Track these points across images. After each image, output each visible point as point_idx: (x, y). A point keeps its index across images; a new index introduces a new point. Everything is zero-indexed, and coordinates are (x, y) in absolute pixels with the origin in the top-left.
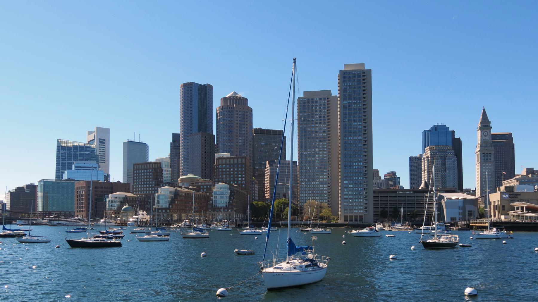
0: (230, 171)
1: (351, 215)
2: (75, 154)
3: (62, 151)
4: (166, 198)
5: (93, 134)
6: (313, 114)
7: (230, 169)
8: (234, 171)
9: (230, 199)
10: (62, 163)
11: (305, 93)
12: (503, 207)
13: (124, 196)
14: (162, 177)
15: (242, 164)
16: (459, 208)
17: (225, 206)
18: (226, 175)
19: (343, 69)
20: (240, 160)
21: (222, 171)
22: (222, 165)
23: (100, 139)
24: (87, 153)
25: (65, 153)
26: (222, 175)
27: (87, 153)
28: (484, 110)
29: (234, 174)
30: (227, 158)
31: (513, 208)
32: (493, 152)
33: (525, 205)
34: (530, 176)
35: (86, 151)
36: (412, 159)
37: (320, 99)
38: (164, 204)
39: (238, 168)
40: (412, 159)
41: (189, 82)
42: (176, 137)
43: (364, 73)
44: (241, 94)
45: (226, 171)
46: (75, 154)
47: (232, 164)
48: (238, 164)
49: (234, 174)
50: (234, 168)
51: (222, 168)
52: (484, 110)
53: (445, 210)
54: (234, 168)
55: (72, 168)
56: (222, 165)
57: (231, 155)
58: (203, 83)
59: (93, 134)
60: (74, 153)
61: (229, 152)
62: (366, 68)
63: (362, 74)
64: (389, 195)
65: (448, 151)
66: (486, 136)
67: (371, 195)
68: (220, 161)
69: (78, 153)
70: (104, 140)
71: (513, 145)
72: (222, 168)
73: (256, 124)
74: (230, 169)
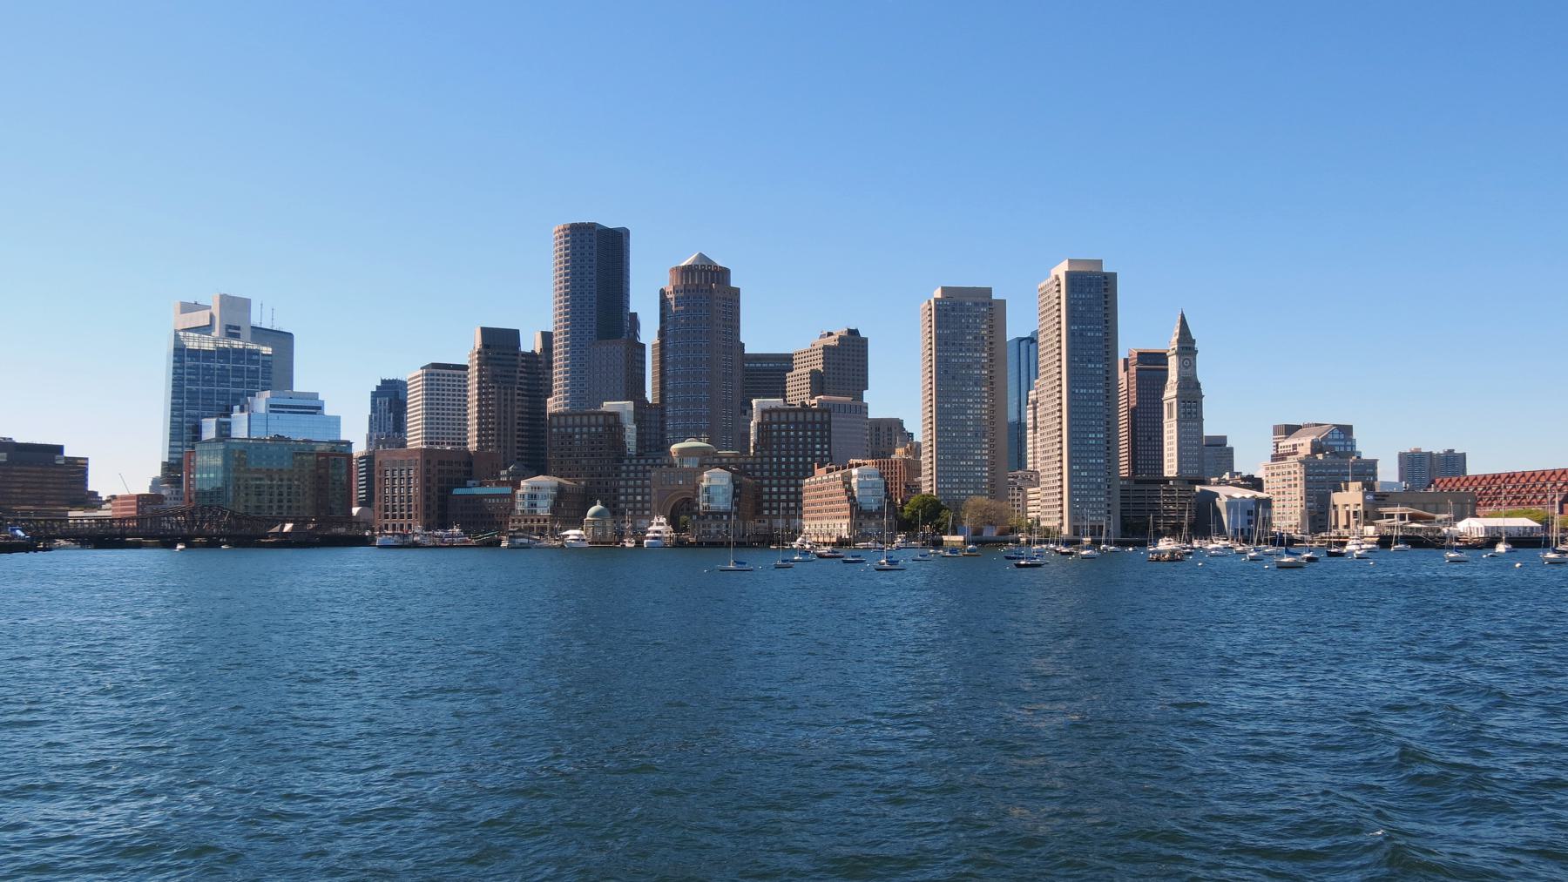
0: (797, 436)
2: (223, 368)
3: (188, 362)
4: (725, 491)
5: (207, 312)
8: (805, 437)
9: (798, 493)
10: (189, 391)
12: (1366, 513)
17: (875, 507)
18: (788, 444)
21: (779, 436)
23: (229, 327)
24: (253, 367)
25: (197, 367)
26: (779, 445)
27: (253, 367)
29: (805, 443)
31: (1380, 516)
33: (1408, 511)
34: (1320, 456)
35: (251, 361)
37: (976, 304)
38: (722, 502)
39: (813, 432)
44: (720, 262)
45: (788, 436)
46: (223, 368)
49: (805, 443)
51: (779, 431)
53: (1225, 516)
54: (805, 431)
56: (779, 423)
59: (207, 312)
60: (217, 365)
62: (1105, 269)
69: (229, 366)
70: (238, 328)
71: (1198, 385)
72: (779, 431)
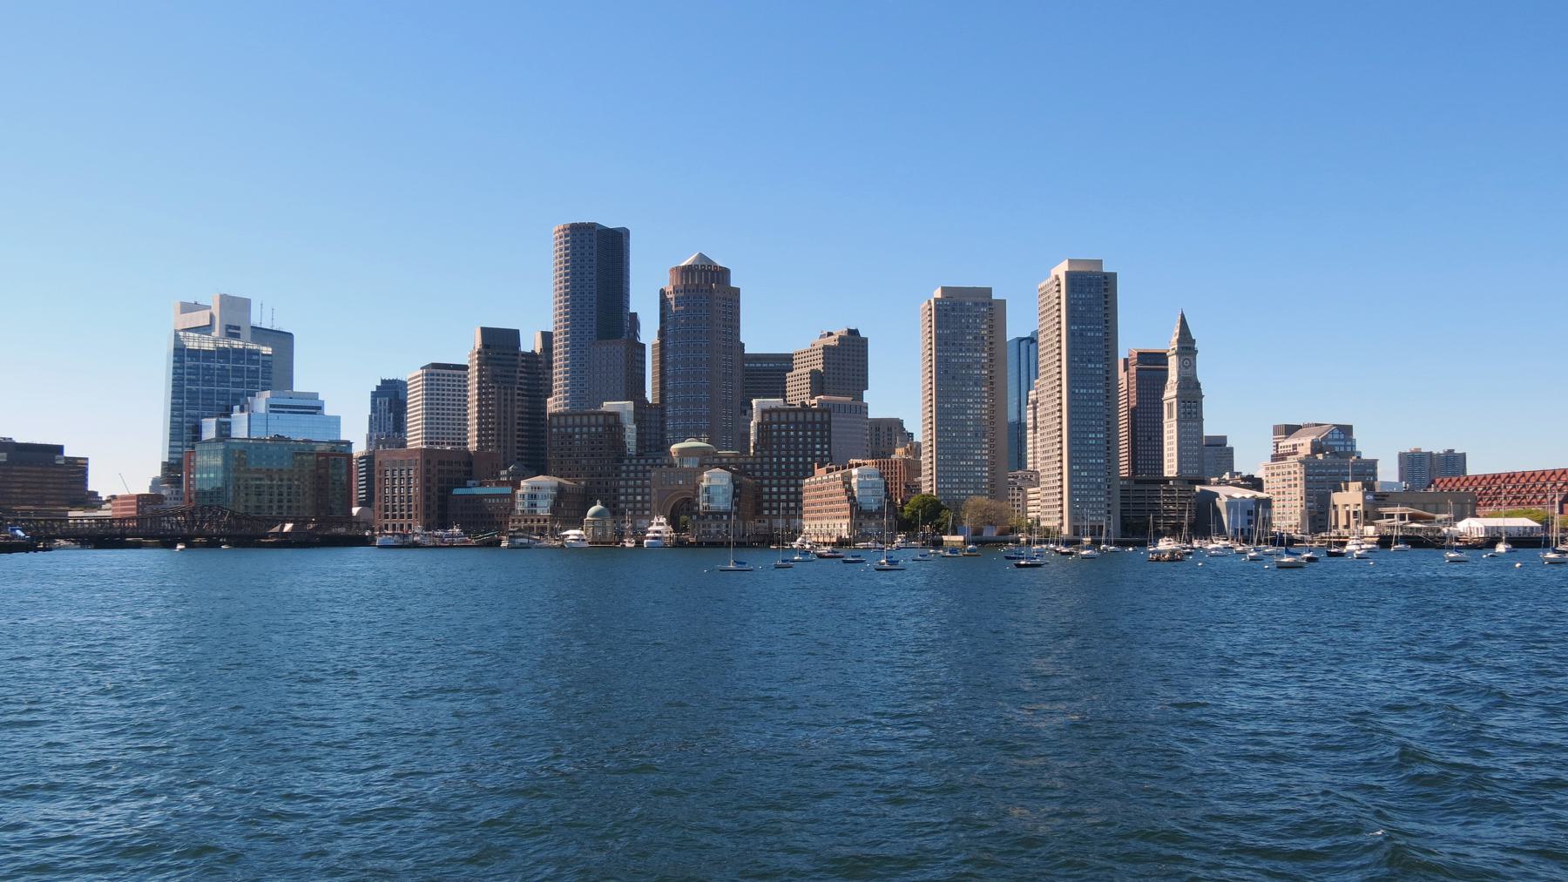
0: (797, 436)
2: (223, 368)
3: (188, 362)
4: (725, 491)
5: (207, 312)
8: (805, 437)
9: (798, 493)
10: (189, 391)
12: (1366, 513)
17: (875, 507)
18: (788, 444)
21: (779, 436)
23: (229, 327)
24: (253, 367)
25: (197, 367)
26: (779, 445)
27: (253, 367)
29: (805, 443)
31: (1380, 516)
33: (1408, 511)
34: (1320, 456)
35: (251, 361)
37: (976, 304)
38: (722, 502)
39: (813, 432)
44: (720, 262)
45: (788, 436)
46: (223, 368)
49: (805, 443)
51: (779, 431)
53: (1225, 516)
54: (805, 431)
56: (779, 423)
59: (207, 312)
60: (217, 365)
62: (1105, 269)
69: (229, 366)
70: (238, 328)
71: (1198, 385)
72: (779, 431)
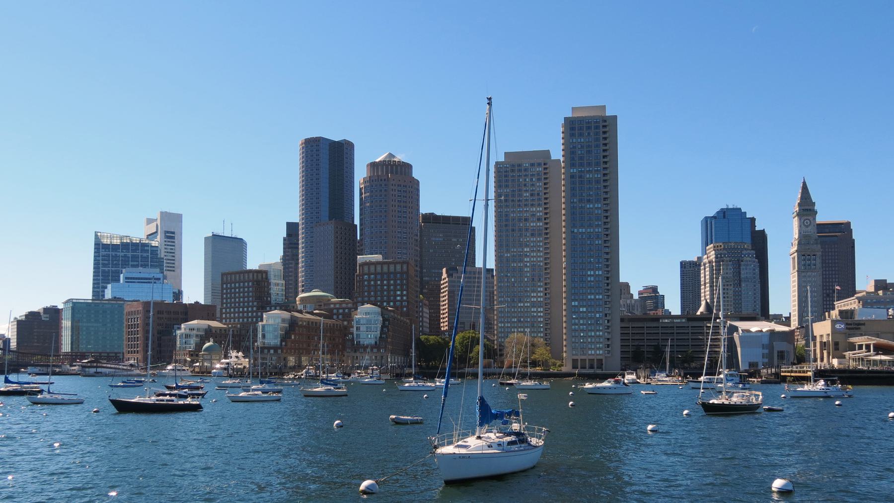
0: (382, 285)
1: (583, 357)
2: (125, 256)
3: (103, 252)
4: (275, 330)
5: (155, 224)
6: (520, 190)
7: (382, 281)
8: (389, 285)
9: (382, 332)
10: (103, 272)
11: (507, 154)
12: (836, 344)
13: (206, 327)
14: (269, 295)
15: (402, 273)
16: (763, 347)
17: (373, 342)
18: (376, 292)
19: (569, 115)
20: (398, 267)
21: (369, 286)
22: (369, 274)
23: (166, 232)
24: (145, 255)
25: (108, 256)
26: (369, 292)
27: (145, 255)
28: (804, 184)
29: (388, 290)
30: (377, 263)
31: (852, 347)
32: (819, 254)
33: (873, 341)
34: (880, 293)
35: (143, 251)
36: (684, 265)
37: (532, 165)
38: (273, 340)
39: (395, 281)
40: (684, 265)
41: (315, 136)
42: (292, 228)
43: (605, 121)
44: (400, 157)
45: (376, 285)
46: (125, 256)
47: (385, 273)
48: (395, 273)
49: (388, 290)
50: (388, 280)
51: (369, 280)
52: (804, 184)
53: (739, 349)
54: (388, 280)
55: (119, 280)
56: (369, 274)
57: (384, 258)
58: (337, 138)
59: (155, 224)
60: (122, 254)
61: (381, 253)
62: (608, 113)
63: (602, 124)
64: (646, 325)
65: (744, 252)
66: (807, 227)
67: (617, 325)
68: (366, 268)
69: (130, 254)
70: (173, 233)
71: (853, 242)
72: (369, 280)
73: (426, 206)
74: (382, 281)
